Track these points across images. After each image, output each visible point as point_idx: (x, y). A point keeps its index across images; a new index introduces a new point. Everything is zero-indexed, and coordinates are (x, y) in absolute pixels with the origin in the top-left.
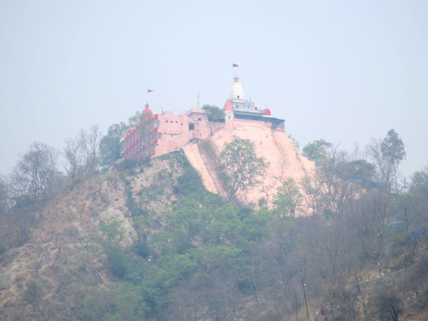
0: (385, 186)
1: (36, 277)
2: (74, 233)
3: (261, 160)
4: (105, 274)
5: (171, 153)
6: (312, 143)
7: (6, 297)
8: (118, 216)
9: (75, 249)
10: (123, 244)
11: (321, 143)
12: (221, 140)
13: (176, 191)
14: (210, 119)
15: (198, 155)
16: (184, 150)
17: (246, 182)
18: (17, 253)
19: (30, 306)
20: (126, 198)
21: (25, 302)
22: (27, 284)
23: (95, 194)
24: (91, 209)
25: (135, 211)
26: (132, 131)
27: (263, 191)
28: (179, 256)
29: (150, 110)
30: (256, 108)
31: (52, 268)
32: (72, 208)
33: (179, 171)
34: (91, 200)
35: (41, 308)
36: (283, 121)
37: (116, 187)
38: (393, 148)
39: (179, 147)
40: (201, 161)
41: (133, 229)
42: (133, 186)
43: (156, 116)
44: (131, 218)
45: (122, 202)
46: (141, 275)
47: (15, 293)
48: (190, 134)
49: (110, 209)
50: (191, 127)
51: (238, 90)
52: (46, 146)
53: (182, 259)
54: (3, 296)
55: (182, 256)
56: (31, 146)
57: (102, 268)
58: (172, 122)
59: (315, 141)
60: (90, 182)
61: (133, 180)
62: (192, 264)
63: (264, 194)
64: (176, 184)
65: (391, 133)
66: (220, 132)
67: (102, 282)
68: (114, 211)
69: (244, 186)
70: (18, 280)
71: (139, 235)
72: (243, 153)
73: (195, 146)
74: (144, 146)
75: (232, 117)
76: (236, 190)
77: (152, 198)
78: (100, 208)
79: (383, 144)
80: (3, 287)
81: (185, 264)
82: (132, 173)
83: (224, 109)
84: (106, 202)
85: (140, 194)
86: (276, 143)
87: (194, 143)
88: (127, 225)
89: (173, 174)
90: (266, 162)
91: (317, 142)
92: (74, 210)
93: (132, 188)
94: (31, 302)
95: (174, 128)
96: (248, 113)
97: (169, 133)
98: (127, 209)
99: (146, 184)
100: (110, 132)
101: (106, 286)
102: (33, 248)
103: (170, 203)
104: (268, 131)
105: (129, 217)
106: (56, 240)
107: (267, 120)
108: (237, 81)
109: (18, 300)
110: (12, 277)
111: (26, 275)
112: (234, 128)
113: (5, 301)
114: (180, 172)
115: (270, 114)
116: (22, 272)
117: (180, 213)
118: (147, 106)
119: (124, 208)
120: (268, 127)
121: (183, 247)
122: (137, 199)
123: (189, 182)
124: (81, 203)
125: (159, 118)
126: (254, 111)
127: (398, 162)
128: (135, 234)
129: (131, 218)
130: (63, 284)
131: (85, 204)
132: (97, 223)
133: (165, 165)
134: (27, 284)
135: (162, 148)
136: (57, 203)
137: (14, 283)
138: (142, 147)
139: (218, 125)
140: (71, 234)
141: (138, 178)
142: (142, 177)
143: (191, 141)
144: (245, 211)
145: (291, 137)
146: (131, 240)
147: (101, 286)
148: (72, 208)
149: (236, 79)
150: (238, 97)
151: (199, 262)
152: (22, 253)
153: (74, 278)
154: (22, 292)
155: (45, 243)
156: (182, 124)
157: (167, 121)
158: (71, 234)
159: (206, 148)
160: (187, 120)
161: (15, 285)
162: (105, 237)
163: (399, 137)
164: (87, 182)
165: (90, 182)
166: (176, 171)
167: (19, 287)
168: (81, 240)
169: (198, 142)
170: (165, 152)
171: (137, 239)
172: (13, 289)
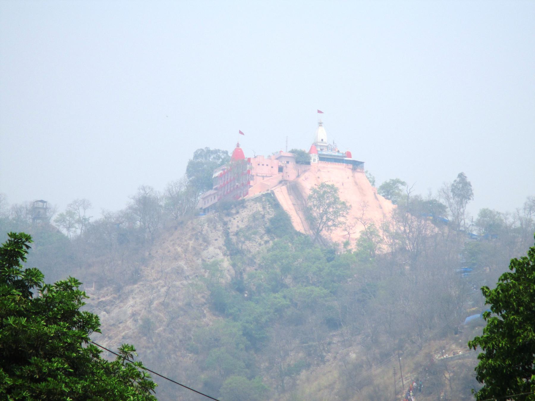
0: (454, 226)
1: (150, 312)
2: (180, 271)
3: (344, 203)
4: (207, 309)
5: (263, 195)
6: (388, 181)
7: (124, 330)
8: (218, 254)
9: (182, 286)
10: (223, 281)
11: (396, 182)
12: (308, 184)
13: (268, 231)
14: (297, 162)
15: (287, 196)
16: (275, 192)
17: (330, 223)
18: (132, 291)
19: (145, 338)
20: (225, 238)
21: (140, 335)
22: (141, 319)
23: (196, 234)
24: (194, 248)
25: (233, 251)
26: (226, 170)
27: (346, 230)
28: (274, 295)
29: (241, 149)
30: (338, 151)
31: (162, 304)
32: (177, 247)
33: (271, 213)
34: (193, 240)
35: (154, 340)
36: (362, 163)
37: (215, 228)
38: (462, 189)
39: (270, 190)
40: (290, 203)
41: (231, 267)
42: (230, 226)
43: (249, 159)
44: (229, 257)
45: (221, 242)
46: (239, 310)
47: (131, 327)
48: (279, 177)
49: (211, 249)
50: (281, 169)
51: (322, 134)
52: (152, 189)
53: (275, 298)
54: (121, 329)
55: (277, 295)
56: (139, 189)
57: (205, 304)
58: (263, 165)
59: (390, 180)
60: (192, 223)
61: (230, 221)
62: (285, 302)
63: (346, 233)
64: (268, 225)
65: (461, 175)
66: (307, 174)
67: (204, 316)
68: (215, 252)
69: (329, 226)
70: (133, 315)
71: (236, 272)
72: (327, 195)
73: (284, 188)
74: (237, 186)
75: (317, 159)
76: (322, 230)
77: (248, 239)
78: (202, 247)
79: (453, 185)
80: (120, 321)
81: (279, 302)
82: (228, 215)
83: (310, 152)
84: (207, 242)
85: (237, 234)
86: (356, 183)
87: (283, 185)
88: (226, 264)
89: (266, 216)
90: (348, 204)
91: (393, 180)
92: (179, 249)
93: (229, 229)
94: (146, 335)
95: (265, 170)
96: (331, 156)
97: (261, 175)
98: (225, 248)
99: (242, 226)
100: (196, 156)
101: (210, 320)
102: (145, 286)
103: (263, 242)
104: (349, 172)
105: (228, 256)
106: (166, 278)
107: (348, 162)
108: (321, 126)
109: (134, 333)
110: (128, 312)
111: (140, 310)
112: (319, 170)
113: (123, 334)
114: (271, 214)
115: (351, 157)
116: (137, 308)
117: (274, 255)
118: (238, 145)
119: (223, 247)
120: (349, 168)
121: (277, 286)
122: (234, 239)
123: (280, 224)
124: (185, 243)
125: (252, 161)
126: (337, 154)
127: (466, 202)
128: (233, 272)
129: (229, 257)
130: (173, 318)
131: (189, 243)
132: (200, 261)
133: (258, 207)
134: (141, 319)
135: (255, 191)
136: (164, 243)
137: (130, 318)
138: (235, 186)
139: (304, 167)
140: (178, 273)
141: (234, 219)
142: (238, 217)
143: (280, 182)
144: (331, 253)
145: (368, 172)
146: (229, 277)
147: (204, 320)
148: (177, 247)
149: (320, 124)
150: (322, 140)
151: (291, 300)
152: (137, 291)
153: (182, 312)
154: (138, 326)
155: (156, 281)
156: (272, 167)
157: (259, 165)
158: (178, 273)
159: (294, 189)
160: (276, 164)
161: (131, 319)
162: (206, 275)
163: (468, 180)
164: (189, 222)
165: (192, 223)
166: (268, 212)
167: (135, 321)
168: (186, 278)
169: (286, 184)
170: (257, 194)
171: (234, 276)
172: (129, 323)
